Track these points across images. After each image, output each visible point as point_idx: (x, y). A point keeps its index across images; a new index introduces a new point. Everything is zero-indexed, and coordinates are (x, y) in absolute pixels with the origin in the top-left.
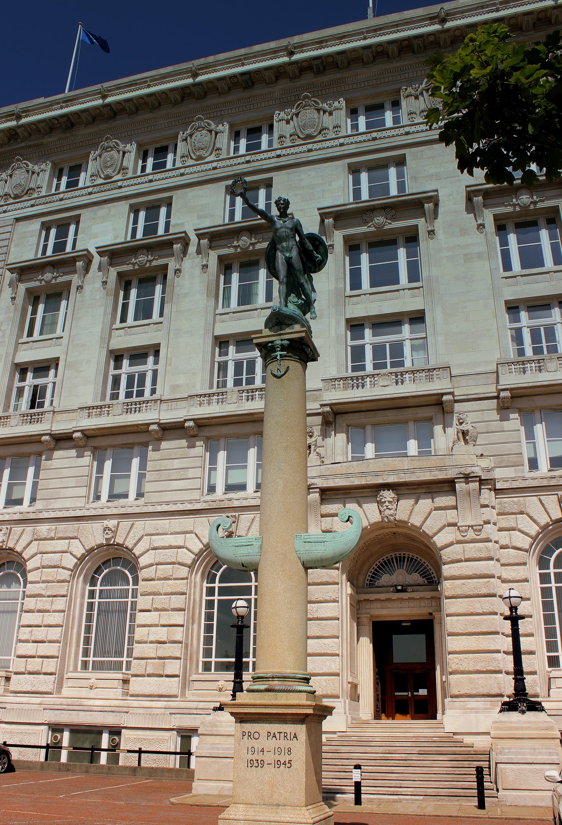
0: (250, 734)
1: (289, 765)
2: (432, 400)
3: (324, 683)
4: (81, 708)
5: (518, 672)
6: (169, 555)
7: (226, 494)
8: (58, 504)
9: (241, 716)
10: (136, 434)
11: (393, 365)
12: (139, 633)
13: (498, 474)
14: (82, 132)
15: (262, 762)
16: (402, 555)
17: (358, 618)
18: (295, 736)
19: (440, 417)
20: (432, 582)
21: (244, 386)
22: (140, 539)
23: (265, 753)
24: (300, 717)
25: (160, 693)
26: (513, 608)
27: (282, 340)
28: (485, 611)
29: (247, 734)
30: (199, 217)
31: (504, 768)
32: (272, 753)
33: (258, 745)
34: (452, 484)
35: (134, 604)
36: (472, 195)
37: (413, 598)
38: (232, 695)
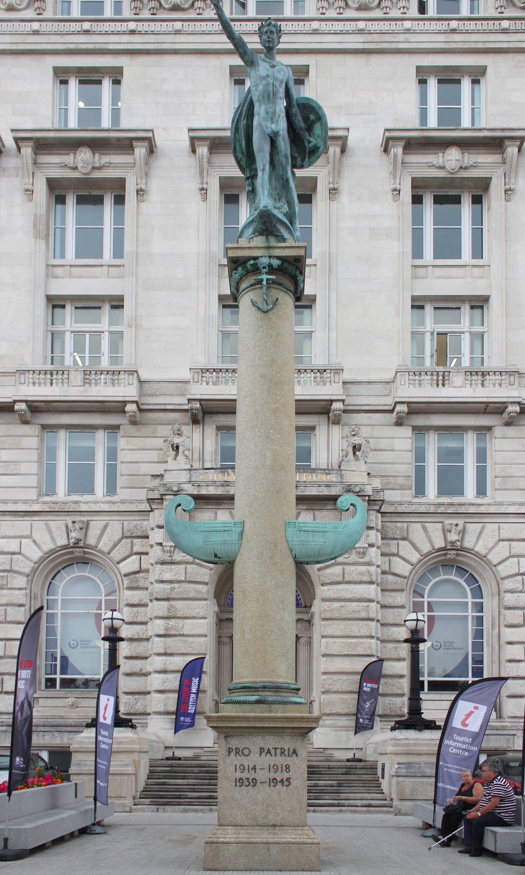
0: (238, 750)
7: (69, 495)
13: (389, 495)
15: (254, 781)
18: (295, 752)
23: (258, 771)
27: (270, 257)
28: (362, 634)
29: (234, 751)
33: (247, 762)
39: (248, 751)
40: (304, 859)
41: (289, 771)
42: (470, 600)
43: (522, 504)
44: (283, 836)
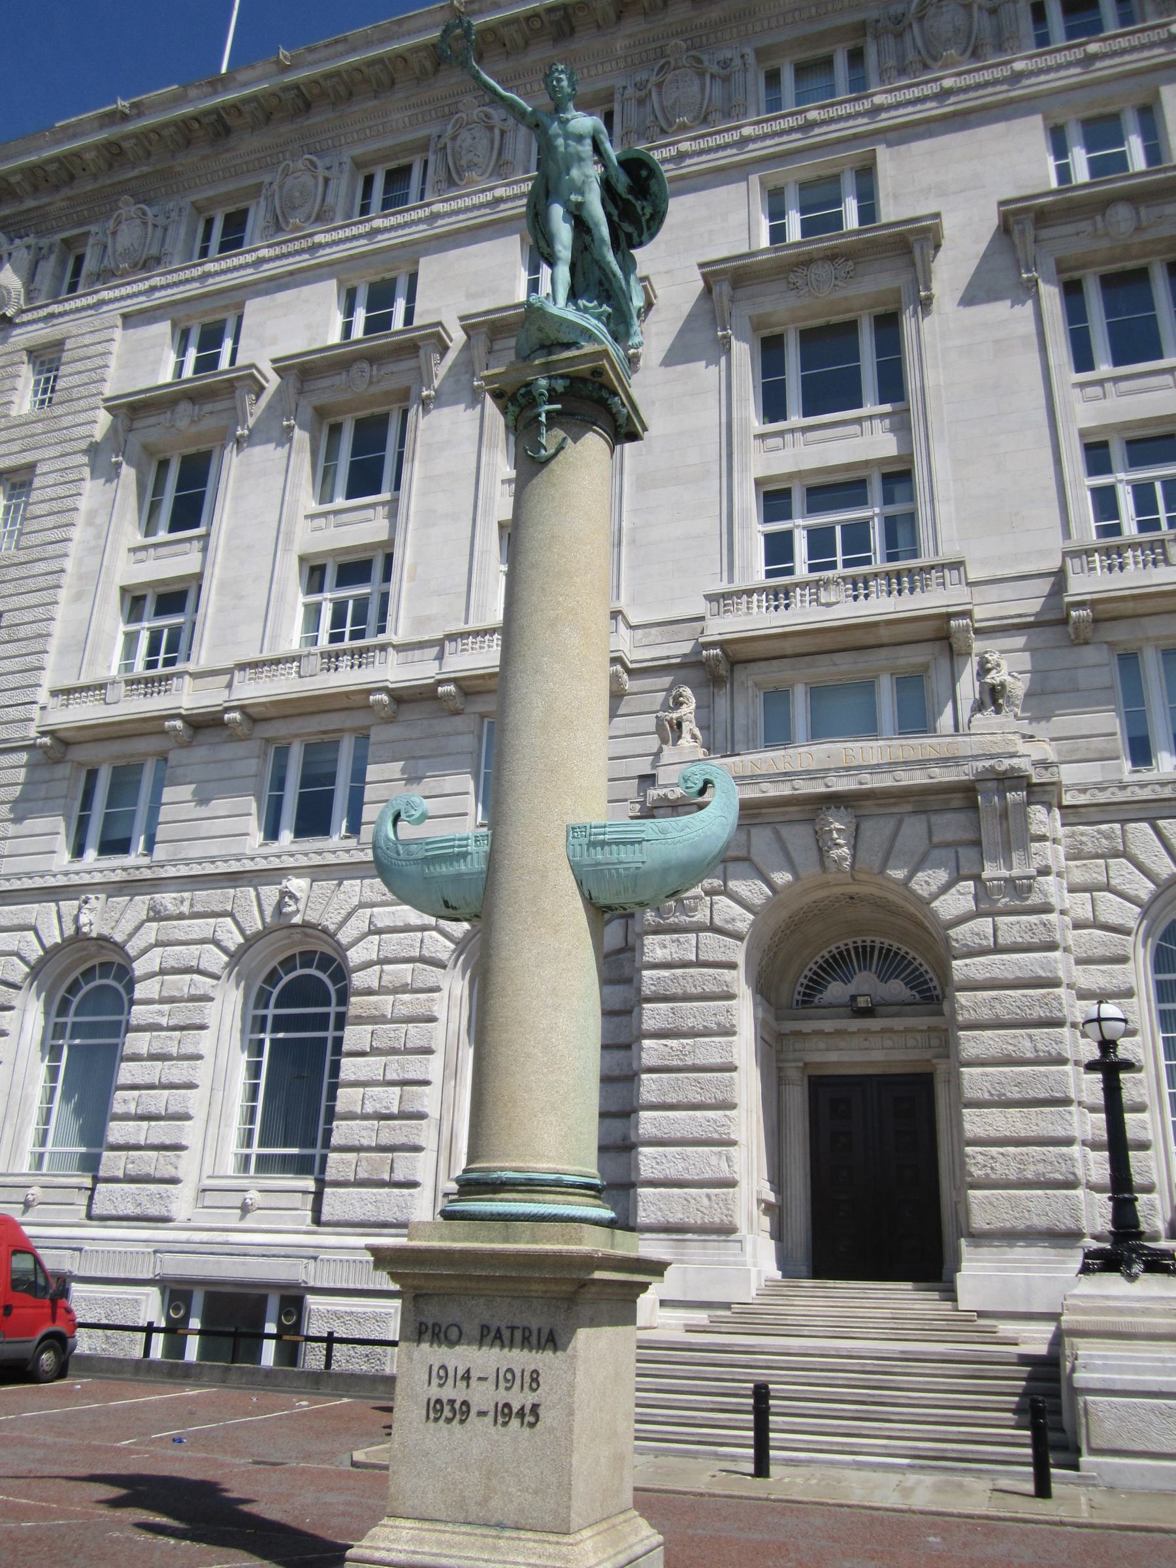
1: (532, 1419)
2: (928, 629)
3: (705, 1202)
4: (226, 1249)
8: (195, 850)
9: (416, 1283)
10: (347, 712)
11: (847, 564)
12: (346, 1099)
13: (1068, 774)
14: (249, 144)
16: (868, 943)
17: (780, 1069)
19: (944, 663)
20: (931, 998)
22: (349, 915)
23: (474, 1382)
24: (564, 1288)
25: (382, 1218)
26: (1107, 1045)
29: (430, 1331)
30: (470, 296)
31: (1094, 1403)
32: (490, 1385)
34: (971, 794)
35: (338, 1041)
36: (1011, 220)
37: (890, 1030)
41: (538, 1385)
44: (511, 1558)
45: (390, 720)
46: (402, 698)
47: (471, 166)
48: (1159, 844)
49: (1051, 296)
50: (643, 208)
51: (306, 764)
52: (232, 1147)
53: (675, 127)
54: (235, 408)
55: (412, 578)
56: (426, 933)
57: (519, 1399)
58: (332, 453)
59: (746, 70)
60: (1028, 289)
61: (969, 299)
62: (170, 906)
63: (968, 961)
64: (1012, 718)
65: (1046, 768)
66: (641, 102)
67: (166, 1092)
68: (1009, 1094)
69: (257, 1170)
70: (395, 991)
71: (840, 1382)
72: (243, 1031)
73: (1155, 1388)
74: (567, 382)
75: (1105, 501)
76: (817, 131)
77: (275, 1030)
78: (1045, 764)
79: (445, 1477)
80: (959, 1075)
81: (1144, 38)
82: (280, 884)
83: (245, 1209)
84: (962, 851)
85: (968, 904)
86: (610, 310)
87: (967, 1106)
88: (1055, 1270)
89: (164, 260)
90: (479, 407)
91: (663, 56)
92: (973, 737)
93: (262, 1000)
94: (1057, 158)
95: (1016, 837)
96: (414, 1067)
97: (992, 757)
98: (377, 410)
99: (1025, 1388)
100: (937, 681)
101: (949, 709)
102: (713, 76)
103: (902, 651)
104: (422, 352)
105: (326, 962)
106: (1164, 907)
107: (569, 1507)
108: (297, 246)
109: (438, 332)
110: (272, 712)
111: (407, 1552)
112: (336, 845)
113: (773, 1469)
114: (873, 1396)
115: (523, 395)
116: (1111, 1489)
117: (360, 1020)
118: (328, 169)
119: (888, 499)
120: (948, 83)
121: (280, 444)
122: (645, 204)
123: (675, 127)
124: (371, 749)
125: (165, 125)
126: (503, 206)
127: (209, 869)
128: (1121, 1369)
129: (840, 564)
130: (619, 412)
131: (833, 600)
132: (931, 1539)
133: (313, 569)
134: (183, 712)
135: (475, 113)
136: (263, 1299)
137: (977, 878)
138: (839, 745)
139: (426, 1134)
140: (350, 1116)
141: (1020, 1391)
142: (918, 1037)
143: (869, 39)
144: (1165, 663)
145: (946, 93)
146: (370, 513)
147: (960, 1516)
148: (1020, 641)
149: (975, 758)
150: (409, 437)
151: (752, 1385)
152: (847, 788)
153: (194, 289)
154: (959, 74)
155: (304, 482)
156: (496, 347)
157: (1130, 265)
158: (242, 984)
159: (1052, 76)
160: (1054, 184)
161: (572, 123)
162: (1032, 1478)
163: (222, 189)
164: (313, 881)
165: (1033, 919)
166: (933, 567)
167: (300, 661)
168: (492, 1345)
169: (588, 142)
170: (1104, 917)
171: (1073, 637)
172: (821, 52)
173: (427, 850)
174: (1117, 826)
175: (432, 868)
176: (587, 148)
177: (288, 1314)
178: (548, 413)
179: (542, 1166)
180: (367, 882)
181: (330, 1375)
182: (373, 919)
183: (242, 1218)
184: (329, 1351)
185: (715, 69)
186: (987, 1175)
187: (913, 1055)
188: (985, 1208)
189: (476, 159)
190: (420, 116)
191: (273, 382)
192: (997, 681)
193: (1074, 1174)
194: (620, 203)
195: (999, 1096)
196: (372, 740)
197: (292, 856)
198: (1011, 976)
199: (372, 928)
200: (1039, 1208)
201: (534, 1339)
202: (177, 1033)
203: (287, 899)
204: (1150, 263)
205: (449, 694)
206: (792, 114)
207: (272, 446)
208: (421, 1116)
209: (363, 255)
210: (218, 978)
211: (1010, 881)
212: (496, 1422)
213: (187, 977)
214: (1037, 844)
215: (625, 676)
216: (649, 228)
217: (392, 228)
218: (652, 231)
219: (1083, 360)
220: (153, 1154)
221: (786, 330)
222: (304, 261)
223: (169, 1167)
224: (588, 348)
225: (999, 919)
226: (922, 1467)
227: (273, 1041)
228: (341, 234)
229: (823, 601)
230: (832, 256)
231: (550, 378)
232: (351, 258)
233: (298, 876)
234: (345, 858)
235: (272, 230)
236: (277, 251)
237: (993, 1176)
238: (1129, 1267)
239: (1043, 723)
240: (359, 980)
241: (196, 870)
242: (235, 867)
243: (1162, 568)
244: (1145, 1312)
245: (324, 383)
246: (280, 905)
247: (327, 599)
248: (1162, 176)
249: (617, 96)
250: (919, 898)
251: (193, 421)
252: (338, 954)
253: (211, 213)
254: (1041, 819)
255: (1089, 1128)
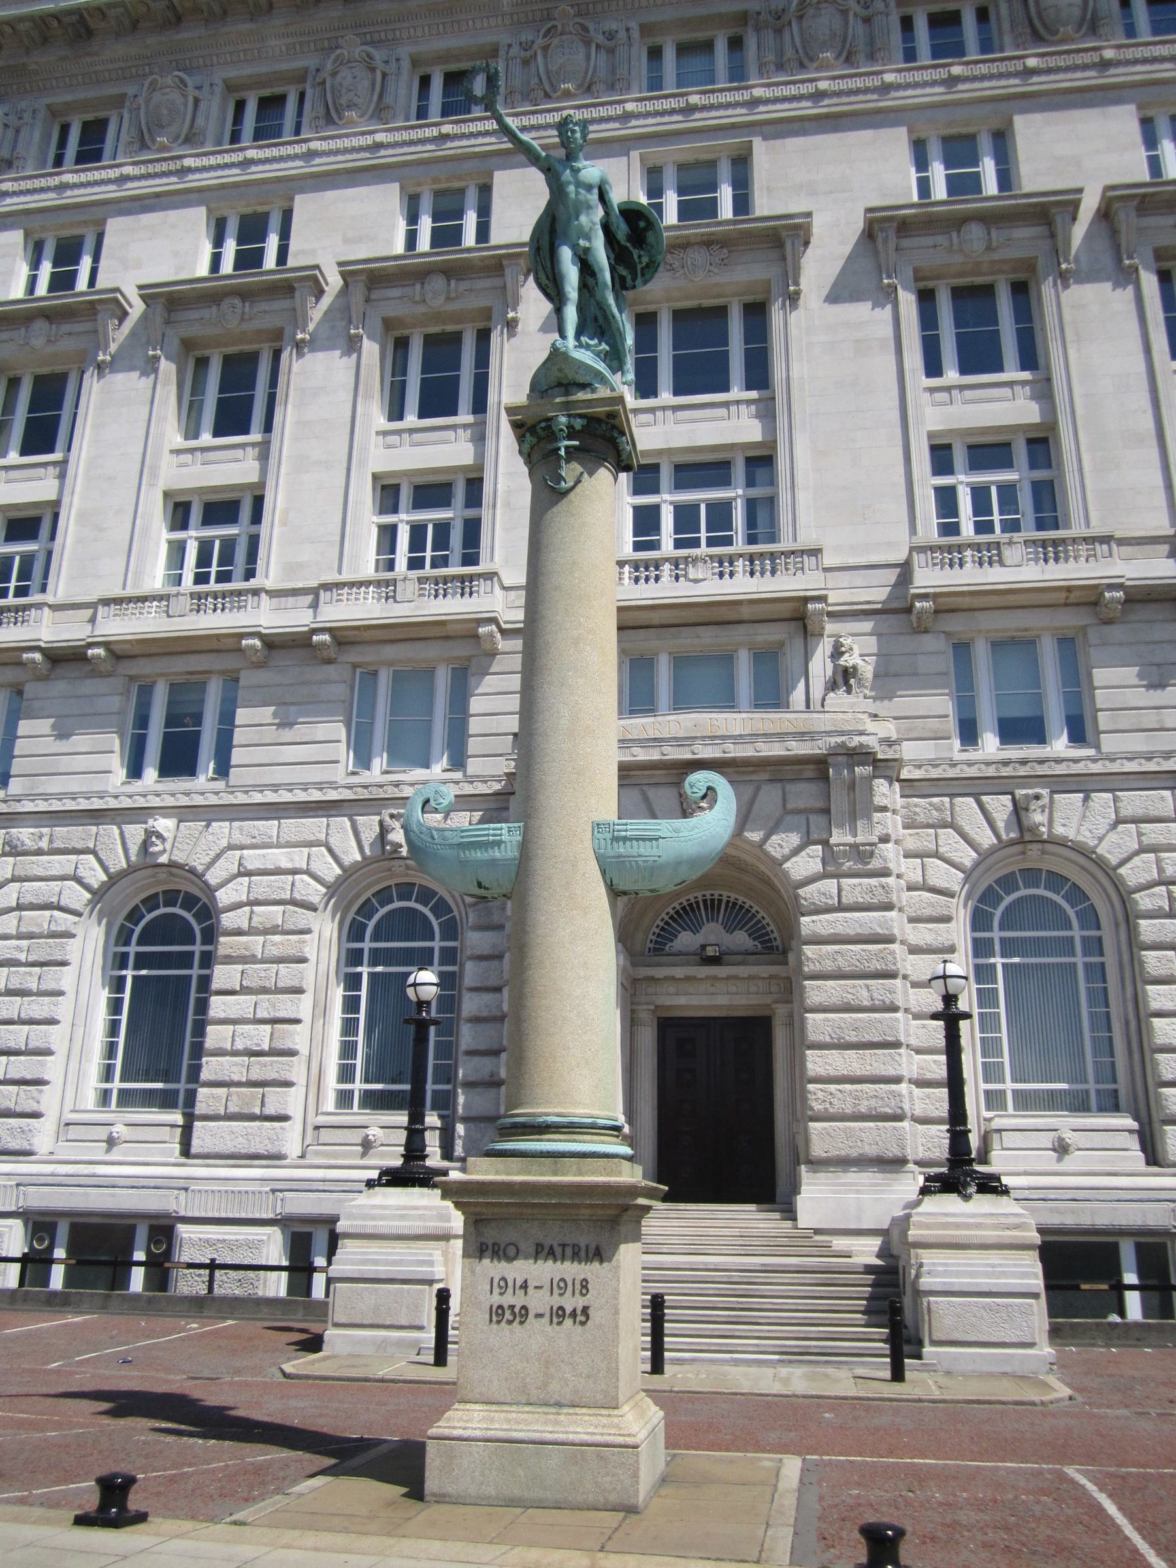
1: (583, 1319)
2: (785, 610)
5: (957, 1114)
6: (279, 886)
9: (477, 1210)
10: (214, 655)
11: (711, 542)
12: (215, 1036)
13: (909, 751)
16: (716, 897)
17: (633, 1011)
19: (798, 643)
20: (771, 948)
21: (428, 571)
22: (218, 857)
23: (530, 1290)
25: (253, 1150)
26: (950, 999)
30: (346, 241)
31: (936, 1302)
34: (822, 766)
36: (876, 226)
37: (736, 978)
38: (403, 1156)
39: (515, 1251)
40: (608, 1479)
42: (1077, 933)
43: (1167, 755)
44: (571, 1429)
45: (260, 665)
46: (274, 644)
47: (350, 106)
48: (982, 817)
49: (908, 301)
50: (640, 257)
51: (170, 704)
52: (92, 1082)
53: (559, 93)
54: (96, 332)
55: (284, 523)
56: (297, 877)
57: (571, 1302)
58: (198, 387)
59: (630, 45)
60: (889, 294)
61: (834, 297)
62: (27, 841)
63: (814, 918)
64: (861, 699)
65: (890, 746)
66: (526, 63)
67: (26, 1028)
68: (847, 1038)
69: (119, 1105)
70: (266, 932)
71: (711, 1292)
72: (104, 968)
73: (986, 1289)
74: (585, 422)
75: (946, 500)
76: (697, 115)
77: (137, 967)
78: (888, 742)
79: (508, 1368)
80: (803, 1021)
81: (1003, 67)
82: (146, 823)
83: (111, 1142)
84: (812, 818)
85: (816, 866)
86: (607, 348)
87: (810, 1047)
88: (883, 1192)
89: (16, 163)
90: (355, 356)
91: (549, 18)
92: (823, 713)
93: (124, 937)
94: (918, 171)
95: (862, 808)
96: (285, 1006)
97: (842, 733)
98: (247, 348)
99: (871, 1293)
100: (792, 657)
101: (801, 685)
102: (598, 47)
103: (762, 628)
104: (297, 294)
105: (190, 901)
106: (985, 872)
107: (617, 1387)
108: (164, 167)
109: (315, 276)
110: (137, 650)
111: (482, 1429)
112: (202, 785)
113: (667, 1368)
114: (742, 1303)
115: (543, 429)
116: (948, 1373)
117: (229, 960)
118: (199, 88)
119: (750, 483)
120: (823, 85)
121: (145, 373)
122: (642, 253)
123: (559, 93)
124: (241, 693)
125: (21, 19)
126: (383, 152)
127: (70, 805)
128: (958, 1274)
129: (703, 542)
130: (624, 449)
131: (701, 577)
132: (827, 1415)
133: (177, 505)
134: (43, 645)
135: (357, 52)
136: (132, 1229)
137: (825, 843)
138: (705, 715)
139: (296, 1070)
140: (220, 1053)
141: (867, 1295)
142: (760, 983)
143: (750, 30)
144: (993, 652)
145: (819, 96)
146: (239, 453)
147: (836, 1398)
148: (867, 626)
149: (829, 733)
150: (282, 379)
151: (649, 1297)
152: (712, 756)
153: (49, 200)
154: (834, 78)
155: (169, 416)
156: (373, 296)
157: (979, 280)
158: (104, 921)
159: (918, 92)
160: (915, 198)
161: (583, 172)
162: (889, 1367)
163: (81, 95)
164: (180, 821)
165: (874, 881)
166: (793, 552)
167: (168, 600)
168: (546, 1260)
169: (596, 191)
170: (933, 881)
171: (915, 625)
172: (701, 35)
173: (462, 837)
174: (947, 799)
175: (467, 852)
176: (594, 197)
177: (157, 1243)
178: (567, 447)
179: (580, 1111)
180: (236, 824)
181: (214, 1299)
182: (243, 861)
183: (108, 1151)
184: (212, 1276)
185: (600, 39)
186: (826, 1109)
187: (755, 1000)
188: (823, 1138)
189: (356, 100)
190: (298, 47)
191: (137, 308)
192: (850, 663)
193: (901, 1108)
194: (616, 247)
195: (838, 1039)
196: (242, 683)
197: (158, 795)
198: (852, 933)
199: (242, 870)
200: (871, 1138)
201: (583, 1254)
202: (37, 969)
203: (154, 839)
204: (995, 281)
205: (323, 644)
206: (674, 96)
207: (136, 374)
208: (292, 1053)
209: (235, 185)
210: (79, 915)
211: (854, 846)
212: (551, 1322)
213: (47, 913)
214: (879, 815)
215: (499, 636)
216: (643, 275)
217: (267, 161)
218: (647, 276)
219: (933, 368)
220: (13, 1089)
221: (660, 309)
222: (172, 184)
223: (30, 1101)
224: (603, 392)
225: (844, 881)
226: (790, 1362)
227: (135, 978)
228: (212, 160)
229: (691, 577)
230: (708, 243)
231: (569, 416)
232: (223, 186)
233: (165, 816)
234: (213, 800)
235: (136, 146)
236: (142, 170)
237: (831, 1110)
238: (965, 1188)
239: (886, 702)
240: (228, 920)
241: (56, 806)
242: (97, 804)
243: (996, 568)
244: (978, 1226)
245: (194, 315)
246: (145, 845)
247: (192, 537)
248: (1013, 202)
249: (502, 53)
250: (773, 859)
251: (49, 341)
252: (205, 893)
253: (68, 119)
254: (884, 792)
255: (915, 1068)
